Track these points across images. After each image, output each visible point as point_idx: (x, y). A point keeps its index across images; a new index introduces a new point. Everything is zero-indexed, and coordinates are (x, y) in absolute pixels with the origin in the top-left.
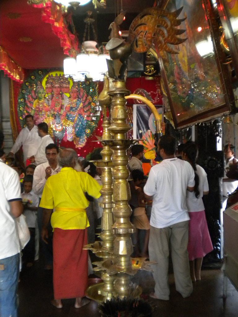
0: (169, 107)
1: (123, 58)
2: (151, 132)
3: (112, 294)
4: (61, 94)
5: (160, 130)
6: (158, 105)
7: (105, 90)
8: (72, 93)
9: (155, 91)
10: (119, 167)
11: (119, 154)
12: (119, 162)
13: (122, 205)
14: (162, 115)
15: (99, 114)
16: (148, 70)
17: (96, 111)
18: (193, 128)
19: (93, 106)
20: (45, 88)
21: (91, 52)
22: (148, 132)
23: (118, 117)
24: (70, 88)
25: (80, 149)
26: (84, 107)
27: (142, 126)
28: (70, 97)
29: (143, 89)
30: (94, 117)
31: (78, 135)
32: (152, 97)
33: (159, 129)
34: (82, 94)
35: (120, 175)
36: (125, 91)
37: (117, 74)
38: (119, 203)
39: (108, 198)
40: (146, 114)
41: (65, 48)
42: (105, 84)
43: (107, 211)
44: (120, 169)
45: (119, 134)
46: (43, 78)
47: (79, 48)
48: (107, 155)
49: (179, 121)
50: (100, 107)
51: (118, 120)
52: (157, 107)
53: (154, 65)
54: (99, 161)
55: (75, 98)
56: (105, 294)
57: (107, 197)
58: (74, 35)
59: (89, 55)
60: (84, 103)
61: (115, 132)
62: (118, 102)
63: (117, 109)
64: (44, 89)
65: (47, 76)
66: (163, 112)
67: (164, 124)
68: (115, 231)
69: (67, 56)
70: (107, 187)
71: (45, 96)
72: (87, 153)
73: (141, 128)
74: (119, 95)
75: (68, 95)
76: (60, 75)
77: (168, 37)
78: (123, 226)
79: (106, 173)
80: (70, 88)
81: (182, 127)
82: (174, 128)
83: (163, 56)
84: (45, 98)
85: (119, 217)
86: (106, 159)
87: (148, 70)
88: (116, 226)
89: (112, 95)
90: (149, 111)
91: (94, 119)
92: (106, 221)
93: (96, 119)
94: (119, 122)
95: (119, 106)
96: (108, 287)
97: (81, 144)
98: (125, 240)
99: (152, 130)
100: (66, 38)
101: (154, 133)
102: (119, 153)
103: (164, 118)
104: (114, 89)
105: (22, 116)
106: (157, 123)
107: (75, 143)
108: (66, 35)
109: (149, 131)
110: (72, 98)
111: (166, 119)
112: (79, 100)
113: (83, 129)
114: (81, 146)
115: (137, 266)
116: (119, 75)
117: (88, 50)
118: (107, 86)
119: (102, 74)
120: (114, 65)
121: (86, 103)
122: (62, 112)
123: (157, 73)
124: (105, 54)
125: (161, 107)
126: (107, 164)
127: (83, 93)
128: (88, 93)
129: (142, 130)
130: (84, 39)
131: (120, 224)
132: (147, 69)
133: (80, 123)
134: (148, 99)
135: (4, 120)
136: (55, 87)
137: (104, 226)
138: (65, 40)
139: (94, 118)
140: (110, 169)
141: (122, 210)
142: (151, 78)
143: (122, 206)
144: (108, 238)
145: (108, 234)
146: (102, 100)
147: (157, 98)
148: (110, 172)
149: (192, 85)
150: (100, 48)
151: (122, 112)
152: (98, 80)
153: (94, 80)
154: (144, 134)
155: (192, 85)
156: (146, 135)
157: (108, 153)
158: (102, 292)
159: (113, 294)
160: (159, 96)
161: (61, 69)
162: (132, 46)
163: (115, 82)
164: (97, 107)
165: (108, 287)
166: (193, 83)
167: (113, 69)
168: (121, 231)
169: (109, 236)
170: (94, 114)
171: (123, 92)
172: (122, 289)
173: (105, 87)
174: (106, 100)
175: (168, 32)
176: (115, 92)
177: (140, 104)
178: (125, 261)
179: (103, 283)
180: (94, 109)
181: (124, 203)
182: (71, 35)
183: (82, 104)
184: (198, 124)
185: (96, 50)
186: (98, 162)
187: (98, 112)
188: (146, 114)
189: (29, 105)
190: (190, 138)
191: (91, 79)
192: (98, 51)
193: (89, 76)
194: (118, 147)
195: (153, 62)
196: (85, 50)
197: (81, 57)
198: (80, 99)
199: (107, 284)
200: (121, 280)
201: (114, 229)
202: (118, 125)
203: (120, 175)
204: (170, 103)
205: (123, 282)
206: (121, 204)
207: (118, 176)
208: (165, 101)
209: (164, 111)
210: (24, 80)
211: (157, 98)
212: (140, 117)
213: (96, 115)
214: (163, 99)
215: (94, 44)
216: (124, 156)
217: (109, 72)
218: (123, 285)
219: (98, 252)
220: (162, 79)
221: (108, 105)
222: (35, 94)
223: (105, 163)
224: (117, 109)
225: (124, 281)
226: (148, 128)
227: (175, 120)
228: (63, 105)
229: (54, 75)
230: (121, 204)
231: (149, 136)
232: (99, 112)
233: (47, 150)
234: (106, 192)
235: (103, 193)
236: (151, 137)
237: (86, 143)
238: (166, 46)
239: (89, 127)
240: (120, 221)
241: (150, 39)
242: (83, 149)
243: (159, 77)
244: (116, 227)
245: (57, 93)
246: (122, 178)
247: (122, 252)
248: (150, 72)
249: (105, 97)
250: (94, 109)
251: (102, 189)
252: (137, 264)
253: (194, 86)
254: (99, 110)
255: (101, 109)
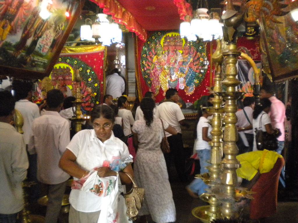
0: (267, 62)
1: (236, 26)
2: (250, 83)
3: (216, 214)
4: (175, 51)
5: (258, 82)
6: (257, 60)
7: (218, 50)
8: (185, 50)
9: (254, 48)
10: (230, 114)
11: (230, 103)
12: (230, 109)
13: (230, 145)
14: (261, 69)
15: (206, 67)
16: (249, 31)
17: (204, 65)
18: (287, 82)
19: (201, 61)
20: (163, 46)
21: (203, 18)
22: (248, 83)
23: (230, 73)
24: (183, 46)
25: (189, 95)
26: (194, 61)
27: (242, 78)
28: (182, 54)
29: (244, 46)
30: (202, 69)
31: (188, 84)
32: (251, 54)
33: (257, 81)
34: (192, 51)
35: (230, 120)
36: (236, 52)
37: (231, 39)
38: (228, 143)
39: (217, 138)
40: (246, 68)
41: (182, 15)
42: (218, 45)
43: (215, 148)
44: (230, 115)
45: (230, 87)
46: (161, 38)
47: (193, 15)
48: (217, 103)
49: (276, 75)
50: (208, 61)
51: (230, 76)
52: (256, 62)
53: (254, 27)
54: (211, 107)
55: (187, 54)
56: (211, 214)
57: (216, 137)
58: (190, 3)
59: (201, 20)
60: (194, 58)
61: (228, 85)
62: (231, 61)
63: (229, 66)
64: (162, 46)
65: (165, 36)
66: (261, 67)
67: (262, 77)
68: (224, 165)
69: (182, 21)
70: (216, 129)
71: (162, 52)
72: (195, 99)
73: (242, 79)
74: (231, 55)
75: (181, 52)
76: (175, 35)
77: (274, 10)
78: (230, 162)
79: (216, 118)
80: (183, 46)
81: (279, 81)
82: (272, 81)
83: (269, 25)
84: (162, 54)
85: (228, 154)
86: (216, 106)
87: (249, 31)
88: (225, 161)
89: (226, 55)
90: (249, 65)
91: (202, 71)
92: (214, 156)
93: (204, 71)
94: (231, 77)
95: (231, 64)
96: (213, 209)
97: (190, 91)
98: (231, 173)
99: (251, 81)
100: (183, 7)
101: (253, 84)
102: (230, 102)
103: (263, 72)
104: (227, 51)
105: (144, 68)
106: (256, 76)
107: (185, 91)
108: (183, 4)
109: (248, 82)
110: (184, 54)
111: (264, 73)
112: (190, 55)
113: (192, 79)
114: (190, 93)
115: (240, 194)
116: (232, 39)
117: (200, 15)
118: (219, 47)
119: (212, 35)
120: (228, 31)
121: (196, 58)
122: (176, 66)
123: (257, 34)
124: (215, 18)
125: (260, 62)
126: (217, 110)
127: (193, 49)
128: (197, 51)
129: (243, 81)
130: (197, 7)
131: (228, 160)
132: (248, 31)
133: (190, 75)
134: (249, 55)
135: (129, 71)
136: (171, 46)
137: (212, 161)
138: (181, 8)
139: (202, 70)
140: (219, 115)
141: (230, 149)
142: (251, 38)
143: (230, 146)
144: (215, 170)
145: (215, 167)
146: (215, 58)
147: (256, 55)
148: (219, 117)
149: (287, 45)
150: (210, 14)
151: (233, 69)
152: (208, 40)
153: (204, 40)
154: (244, 85)
155: (287, 45)
156: (246, 86)
157: (218, 101)
158: (208, 213)
159: (217, 215)
160: (258, 53)
161: (177, 30)
162: (243, 16)
163: (229, 44)
164: (206, 62)
165: (213, 209)
166: (288, 43)
167: (228, 36)
168: (229, 166)
169: (216, 169)
170: (202, 67)
171: (235, 53)
172: (227, 211)
173: (217, 47)
174: (218, 58)
175: (274, 5)
176: (228, 53)
177: (242, 59)
178: (230, 190)
179: (209, 206)
180: (202, 63)
181: (233, 143)
182: (187, 4)
183: (192, 59)
184: (294, 79)
185: (207, 15)
186: (210, 109)
187: (206, 65)
188: (246, 68)
189: (150, 59)
190: (284, 89)
191: (202, 39)
192: (209, 16)
193: (201, 37)
194: (229, 97)
195: (254, 25)
196: (198, 15)
197: (194, 21)
198: (191, 55)
199: (212, 206)
200: (226, 204)
201: (223, 163)
202: (230, 80)
203: (230, 120)
204: (268, 58)
205: (228, 206)
206: (230, 144)
207: (229, 121)
208: (263, 57)
209: (263, 65)
210: (147, 39)
211: (256, 55)
212: (241, 70)
213: (204, 68)
214: (261, 56)
215: (205, 10)
216: (234, 104)
217: (224, 36)
218: (228, 208)
219: (207, 181)
220: (261, 39)
221: (221, 62)
222: (155, 51)
223: (216, 109)
224: (229, 66)
225: (229, 205)
226: (247, 80)
227: (272, 74)
228: (177, 60)
229: (170, 36)
230: (230, 144)
231: (248, 87)
232: (207, 66)
233: (249, 124)
234: (215, 133)
235: (213, 133)
236: (250, 87)
237: (195, 91)
238: (272, 17)
239: (198, 77)
240: (228, 157)
241: (258, 10)
242: (192, 96)
243: (259, 38)
244: (225, 162)
245: (172, 50)
246: (231, 123)
247: (229, 182)
248: (250, 33)
249: (218, 56)
250: (202, 63)
251: (212, 131)
252: (240, 193)
253: (288, 45)
254: (206, 64)
255: (208, 64)
